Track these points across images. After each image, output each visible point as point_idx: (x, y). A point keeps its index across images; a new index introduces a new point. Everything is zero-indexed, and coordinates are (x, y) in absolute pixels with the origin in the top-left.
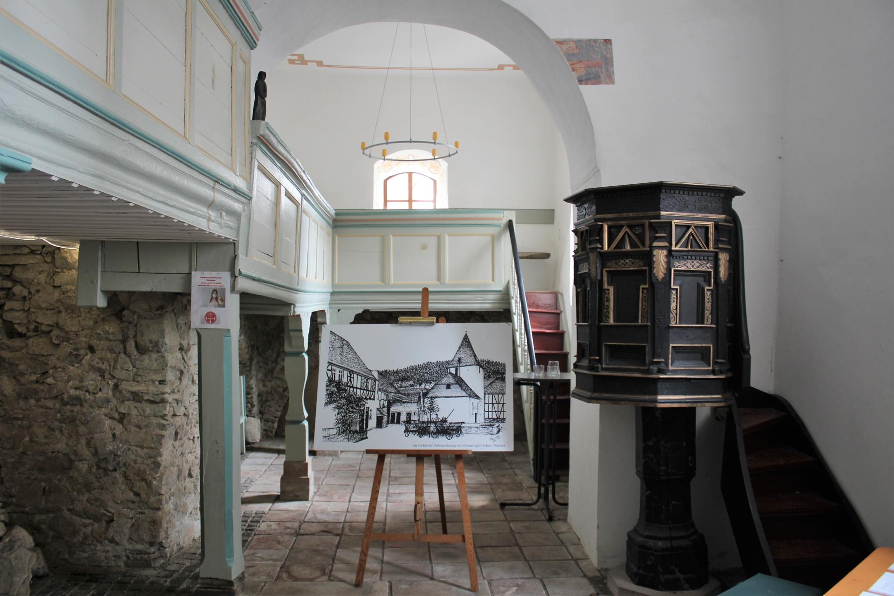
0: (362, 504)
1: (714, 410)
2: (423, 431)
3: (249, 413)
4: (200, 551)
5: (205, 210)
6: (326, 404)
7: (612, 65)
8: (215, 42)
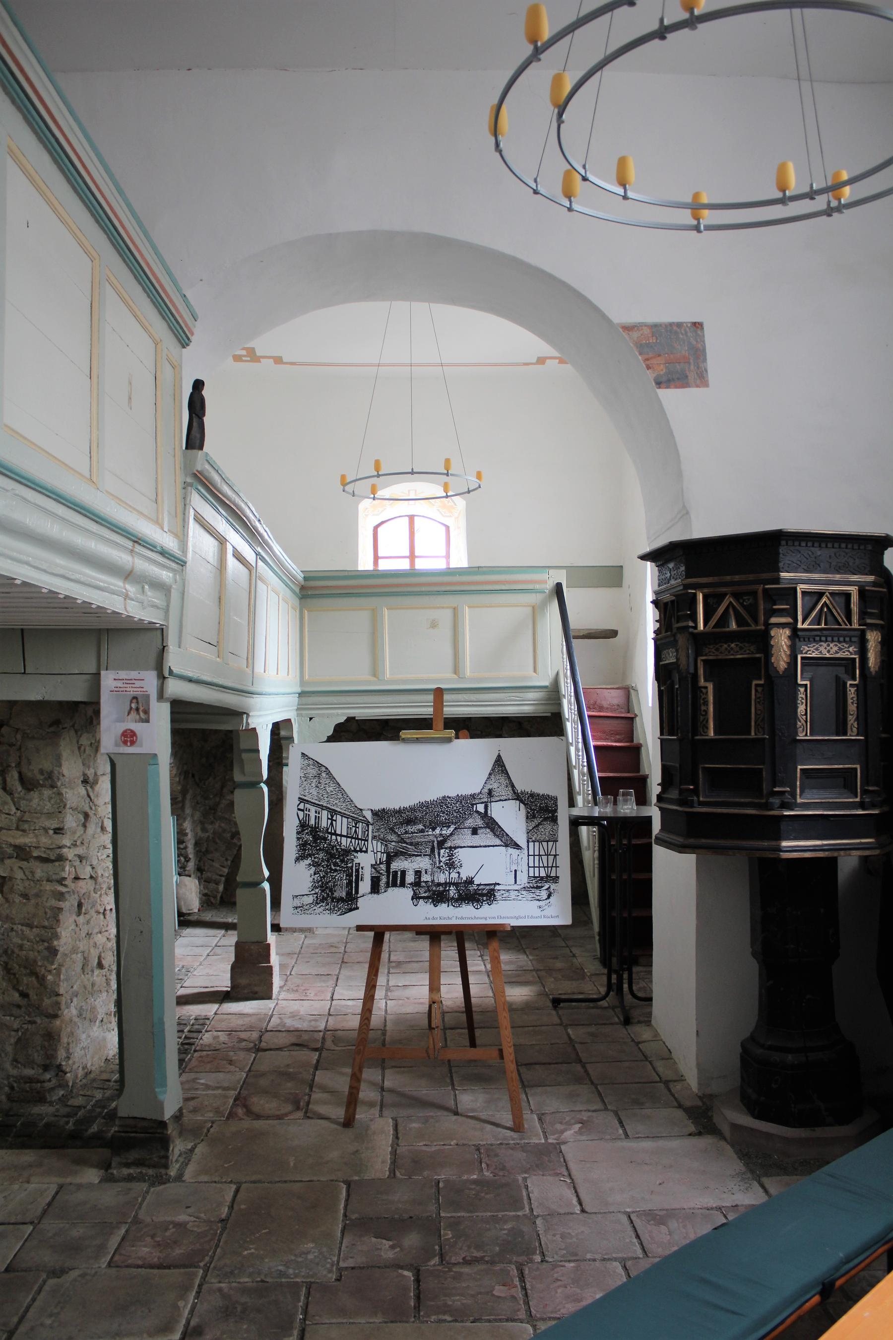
0: (350, 1003)
1: (864, 860)
2: (438, 896)
3: (182, 871)
4: (116, 1076)
5: (121, 584)
6: (297, 860)
7: (705, 360)
8: (131, 335)
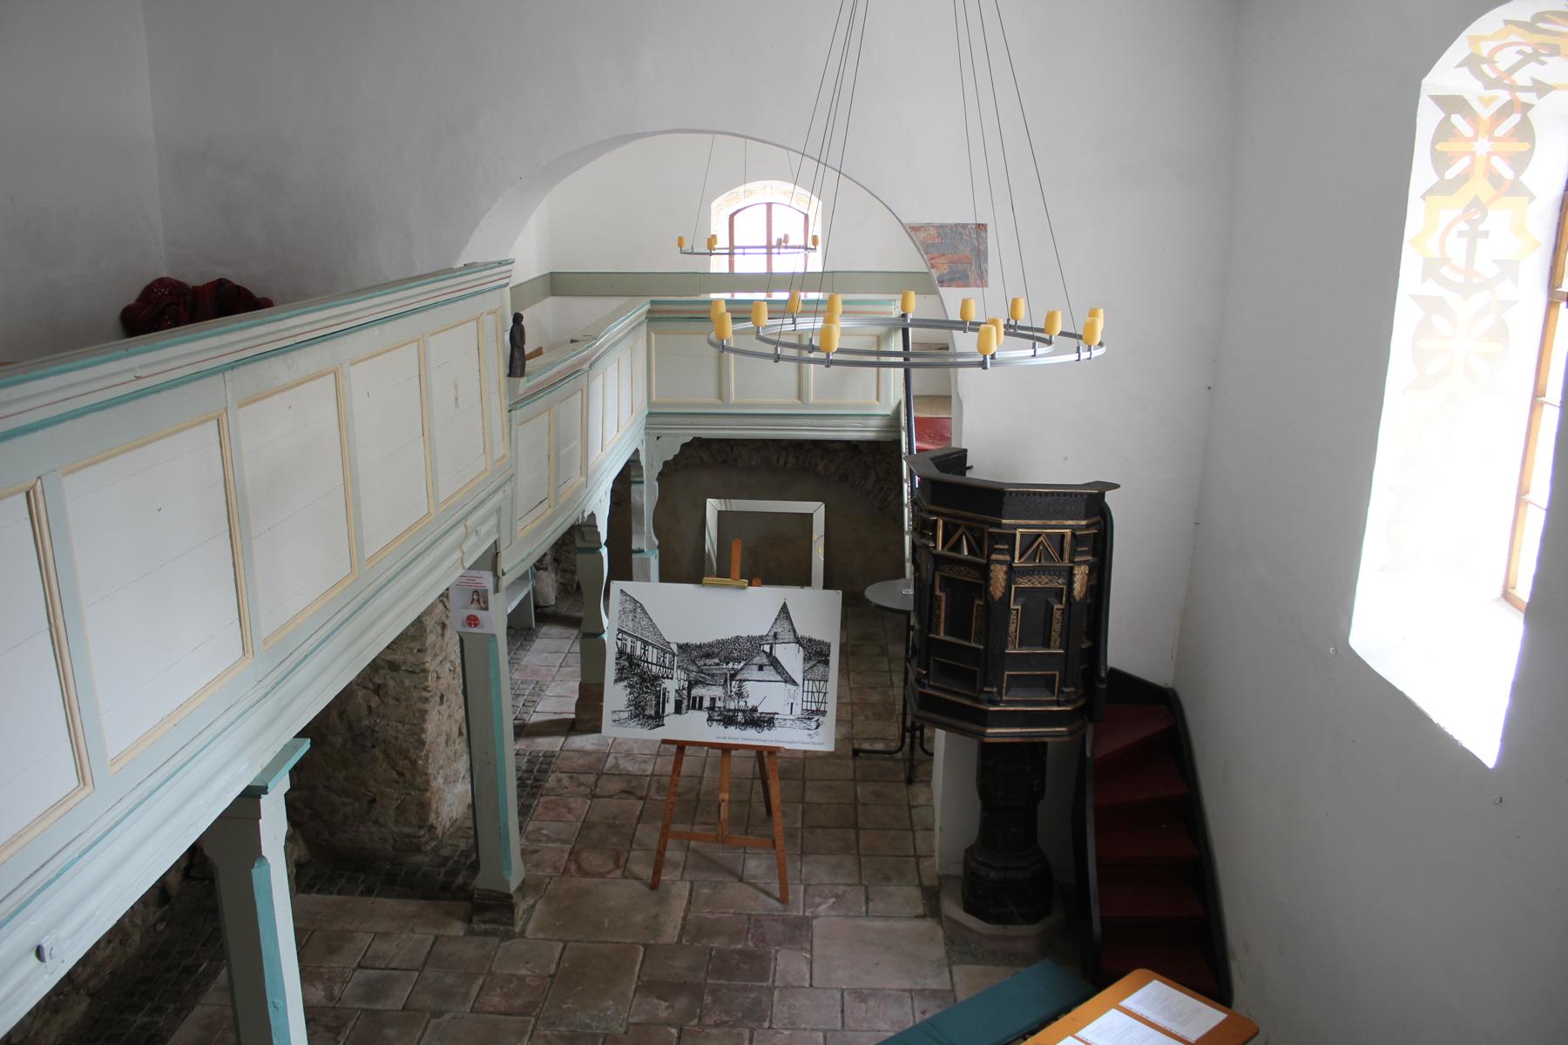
2: (728, 720)
6: (616, 681)
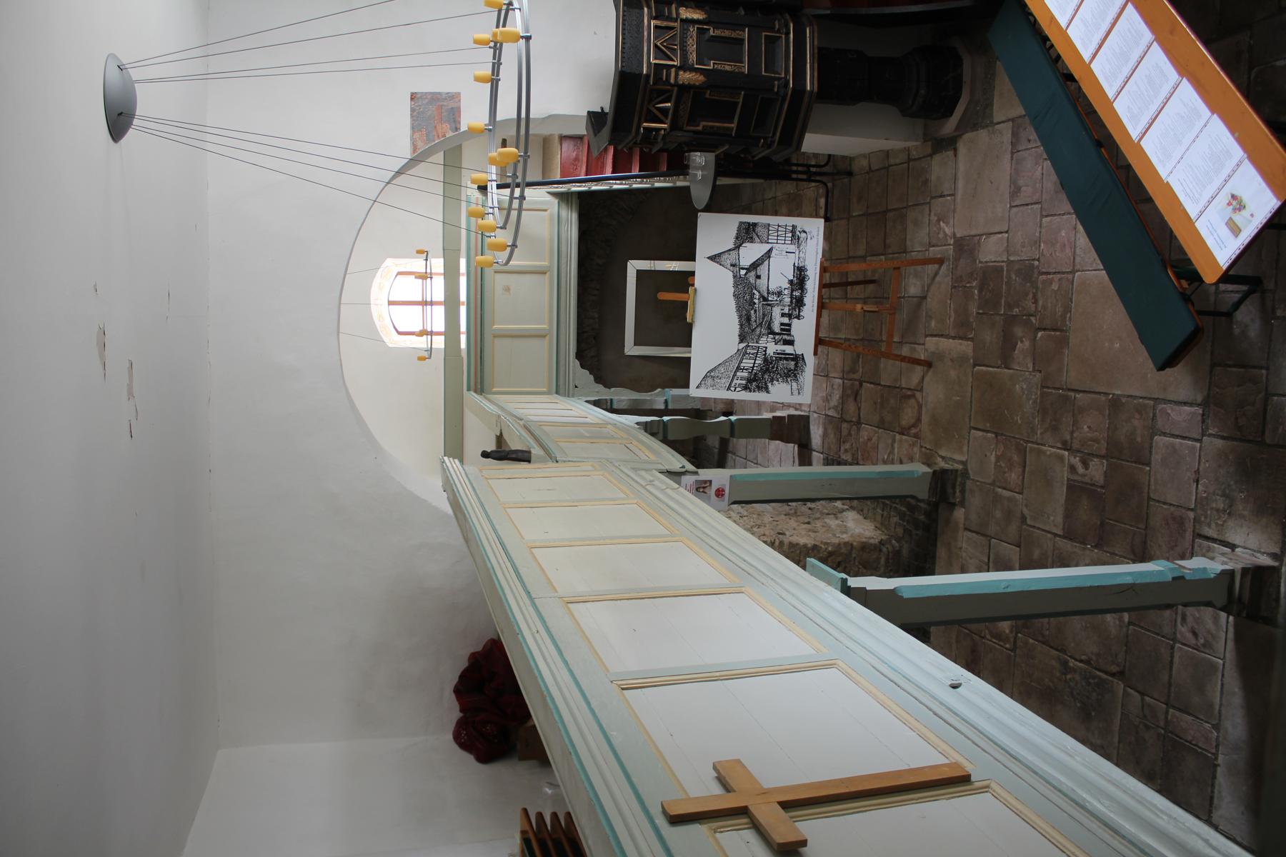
2: (799, 303)
